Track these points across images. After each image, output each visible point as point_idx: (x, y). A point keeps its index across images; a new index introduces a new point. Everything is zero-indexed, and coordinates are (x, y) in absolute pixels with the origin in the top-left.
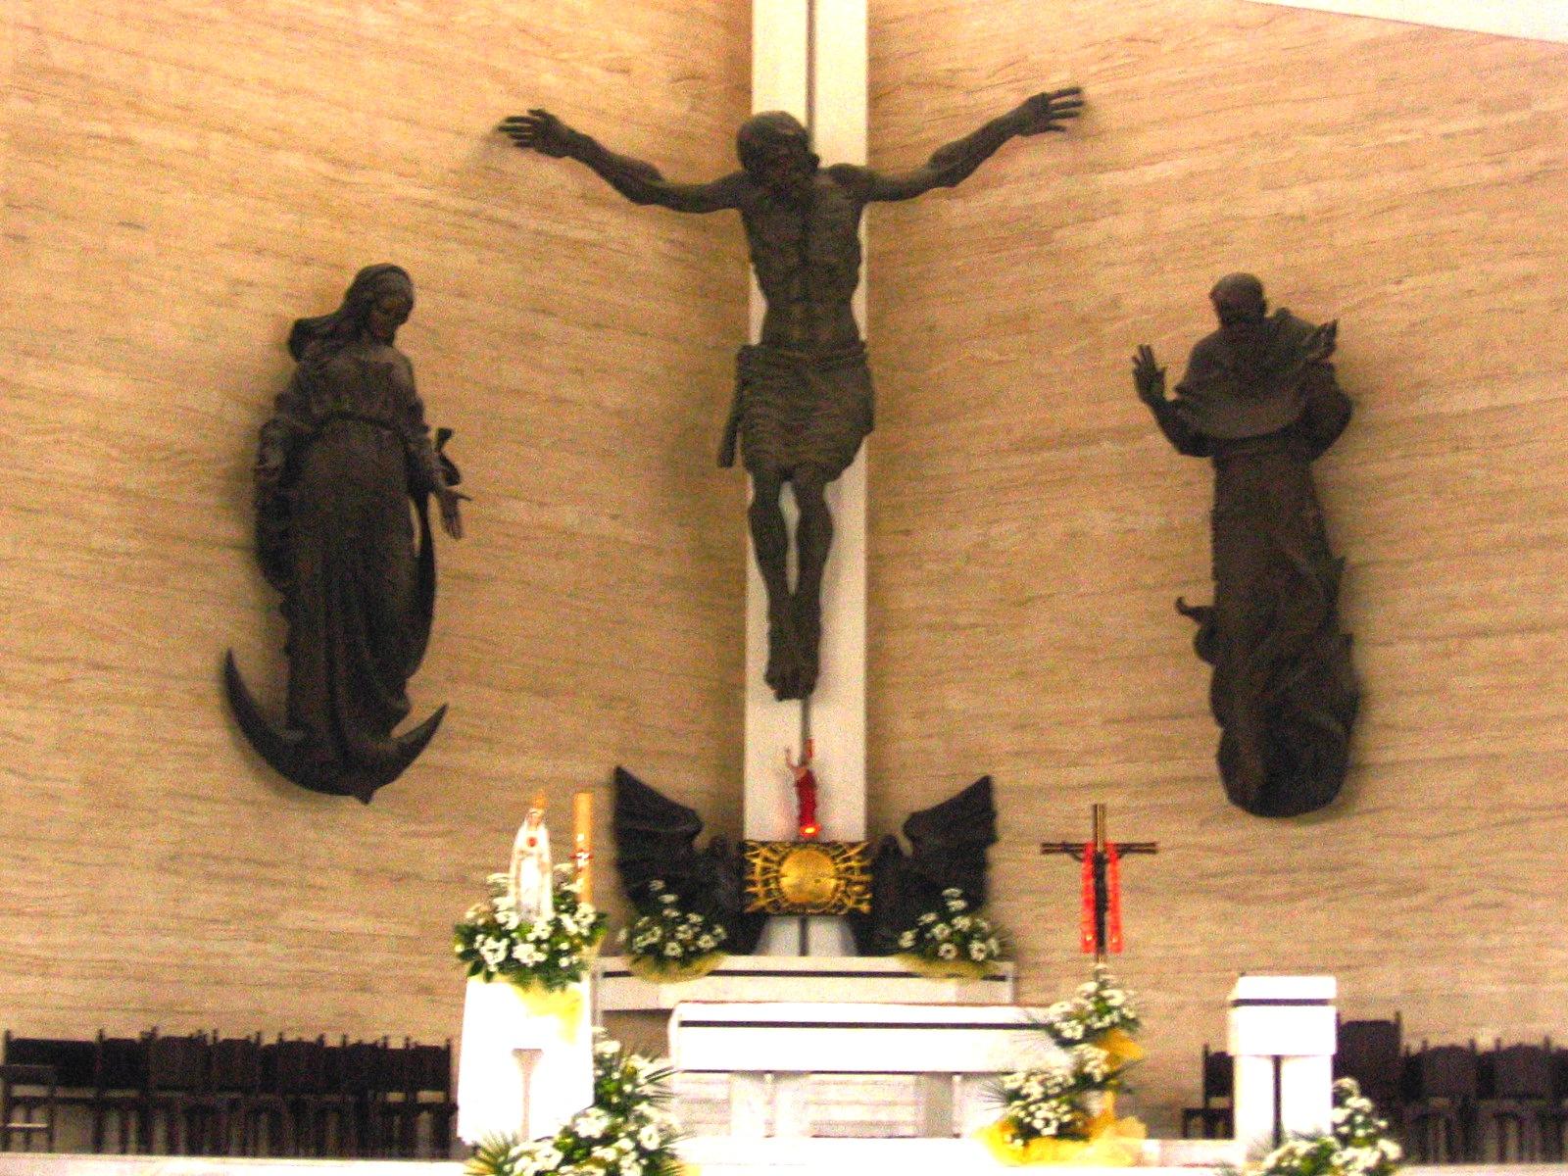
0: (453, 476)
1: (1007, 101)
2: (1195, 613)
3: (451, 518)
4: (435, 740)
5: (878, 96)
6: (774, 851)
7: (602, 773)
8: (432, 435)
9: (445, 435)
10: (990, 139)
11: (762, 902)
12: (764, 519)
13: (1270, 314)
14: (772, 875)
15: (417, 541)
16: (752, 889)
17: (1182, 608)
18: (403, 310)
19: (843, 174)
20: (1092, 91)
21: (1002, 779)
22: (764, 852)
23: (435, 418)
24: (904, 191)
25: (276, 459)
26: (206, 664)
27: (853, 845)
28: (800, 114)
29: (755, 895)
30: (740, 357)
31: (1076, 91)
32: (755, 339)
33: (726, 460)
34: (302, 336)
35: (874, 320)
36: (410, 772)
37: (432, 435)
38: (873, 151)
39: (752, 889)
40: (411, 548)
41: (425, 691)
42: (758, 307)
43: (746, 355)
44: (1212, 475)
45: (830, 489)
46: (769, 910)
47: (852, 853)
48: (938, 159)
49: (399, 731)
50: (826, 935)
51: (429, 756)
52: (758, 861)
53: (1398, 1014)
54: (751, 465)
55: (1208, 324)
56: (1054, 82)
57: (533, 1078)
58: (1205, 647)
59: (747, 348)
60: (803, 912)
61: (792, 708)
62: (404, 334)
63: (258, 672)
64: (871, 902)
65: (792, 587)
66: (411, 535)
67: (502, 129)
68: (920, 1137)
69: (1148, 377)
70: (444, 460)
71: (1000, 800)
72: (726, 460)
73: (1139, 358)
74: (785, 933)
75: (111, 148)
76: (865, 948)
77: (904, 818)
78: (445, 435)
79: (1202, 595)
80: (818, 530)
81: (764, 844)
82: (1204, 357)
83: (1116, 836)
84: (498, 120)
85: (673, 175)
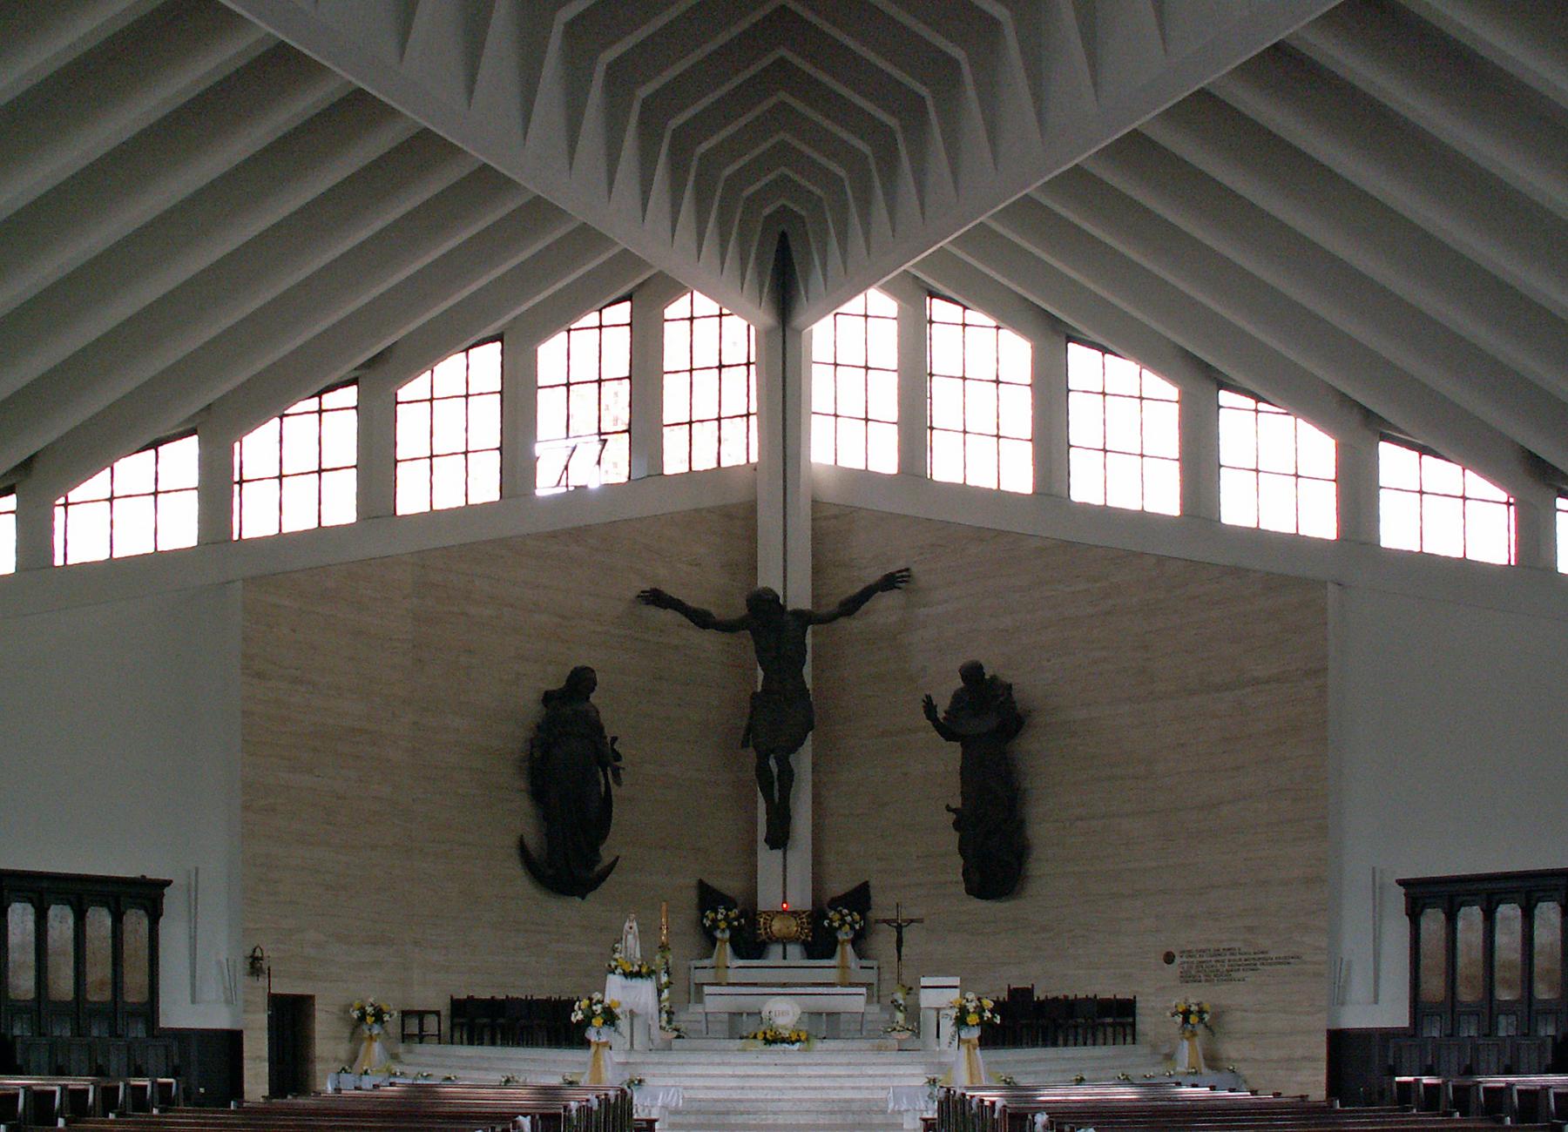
0: (618, 757)
1: (874, 575)
2: (954, 811)
3: (616, 775)
4: (615, 869)
5: (817, 571)
6: (769, 916)
7: (694, 882)
8: (609, 739)
9: (614, 739)
10: (867, 594)
11: (764, 937)
12: (762, 771)
13: (987, 677)
14: (768, 926)
15: (603, 789)
16: (759, 932)
17: (948, 808)
18: (592, 685)
19: (798, 614)
20: (914, 569)
21: (873, 883)
22: (764, 916)
23: (609, 732)
24: (830, 618)
25: (537, 754)
26: (512, 840)
27: (804, 912)
28: (778, 589)
29: (761, 934)
30: (752, 698)
31: (907, 570)
32: (759, 689)
33: (745, 745)
34: (548, 698)
35: (815, 678)
36: (604, 885)
37: (609, 739)
38: (816, 597)
39: (759, 932)
40: (600, 793)
41: (606, 854)
42: (760, 673)
43: (755, 696)
44: (960, 749)
45: (792, 758)
46: (767, 940)
47: (804, 916)
48: (843, 604)
49: (598, 868)
50: (794, 950)
51: (613, 876)
52: (762, 920)
53: (1401, 883)
54: (755, 748)
55: (958, 683)
56: (899, 565)
57: (1471, 497)
58: (957, 825)
59: (754, 693)
60: (784, 941)
61: (778, 853)
62: (593, 698)
63: (532, 842)
64: (812, 937)
65: (777, 800)
66: (599, 784)
67: (638, 596)
68: (829, 1039)
69: (929, 708)
70: (614, 750)
71: (872, 892)
72: (745, 745)
73: (925, 699)
74: (776, 950)
75: (410, 130)
76: (810, 956)
77: (828, 899)
78: (614, 739)
79: (957, 803)
80: (787, 776)
81: (764, 912)
82: (957, 697)
83: (905, 915)
84: (637, 591)
85: (717, 612)
